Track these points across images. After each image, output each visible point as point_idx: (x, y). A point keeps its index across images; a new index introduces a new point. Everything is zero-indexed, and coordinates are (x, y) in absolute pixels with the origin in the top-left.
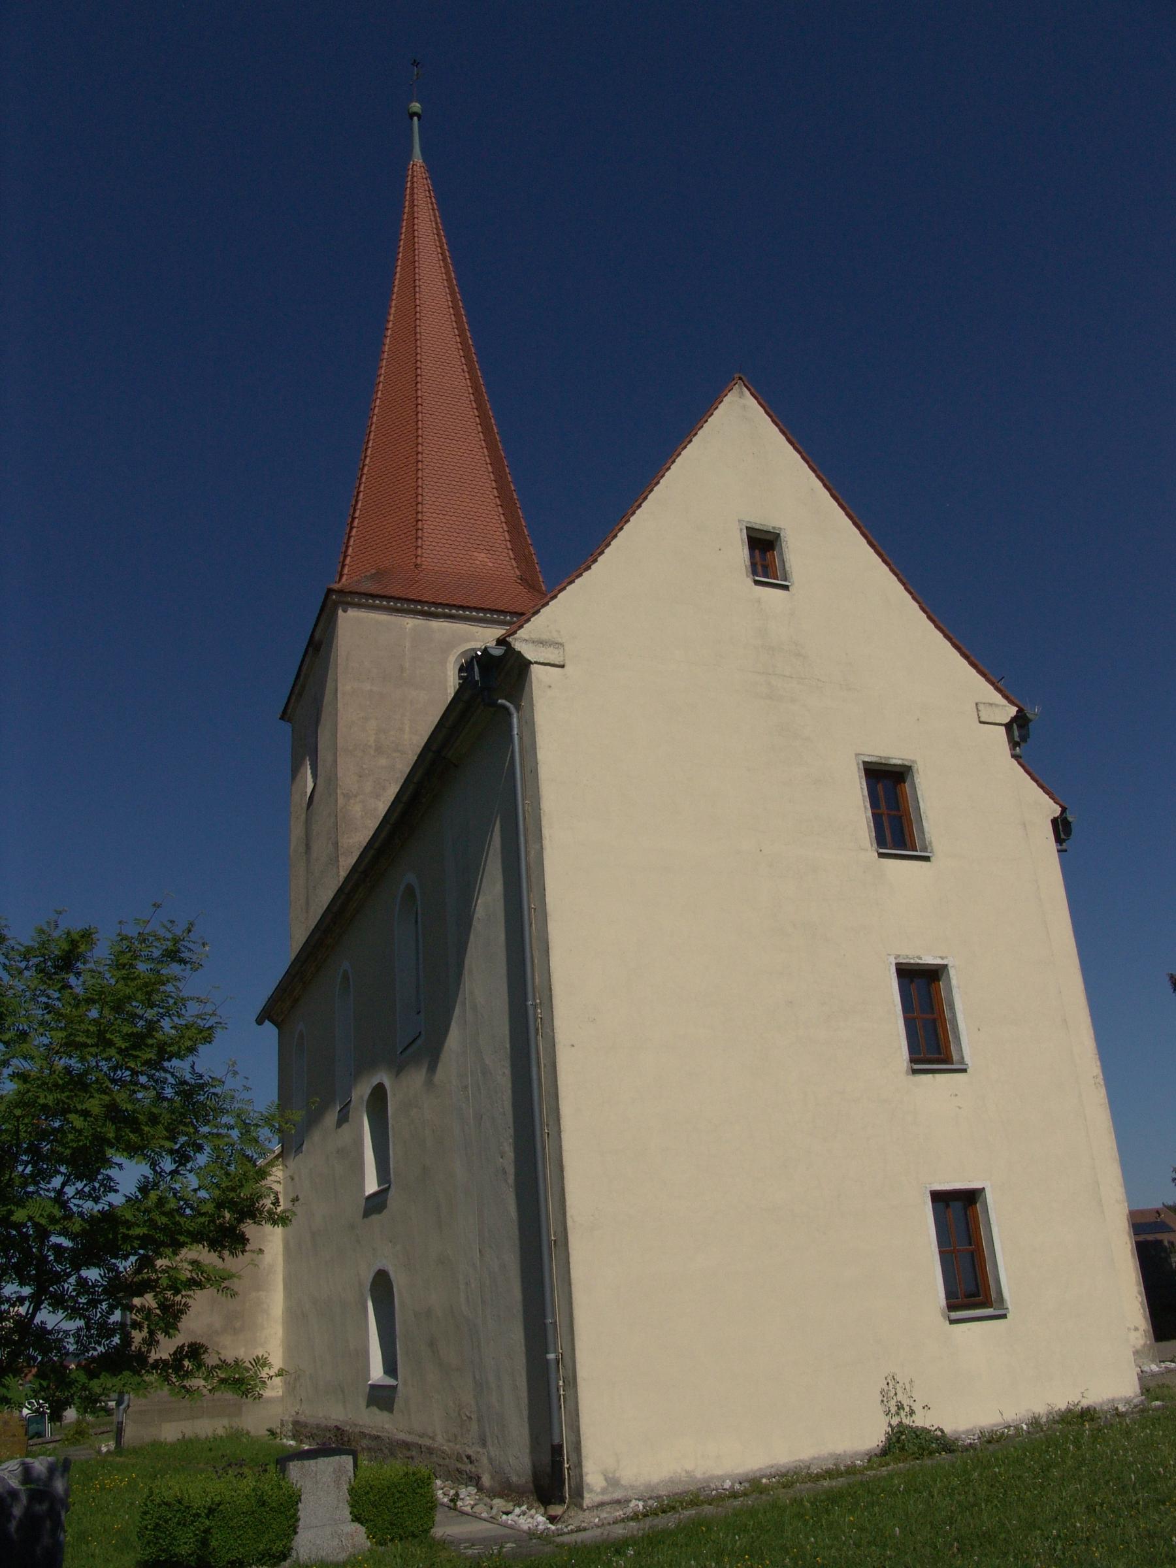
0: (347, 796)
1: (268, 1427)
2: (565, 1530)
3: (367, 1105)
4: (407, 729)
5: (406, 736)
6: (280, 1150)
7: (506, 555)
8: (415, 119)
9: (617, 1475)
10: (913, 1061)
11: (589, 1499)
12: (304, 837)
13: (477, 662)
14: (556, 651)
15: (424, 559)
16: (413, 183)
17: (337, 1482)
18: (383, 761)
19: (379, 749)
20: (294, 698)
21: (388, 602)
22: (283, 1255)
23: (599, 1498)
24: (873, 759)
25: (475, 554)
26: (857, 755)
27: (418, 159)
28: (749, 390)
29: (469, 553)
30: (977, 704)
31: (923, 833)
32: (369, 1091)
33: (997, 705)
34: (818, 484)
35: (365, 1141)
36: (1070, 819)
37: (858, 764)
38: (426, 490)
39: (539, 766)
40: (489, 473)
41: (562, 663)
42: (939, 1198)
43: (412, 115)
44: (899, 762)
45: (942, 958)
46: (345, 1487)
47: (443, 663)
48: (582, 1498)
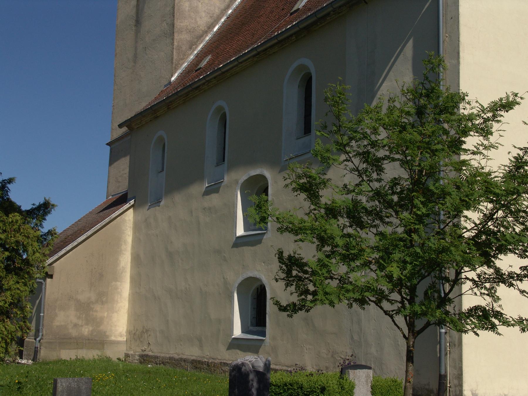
1: (118, 357)
6: (133, 203)
9: (477, 392)
12: (135, 16)
17: (367, 381)
22: (131, 263)
32: (245, 177)
35: (238, 207)
39: (460, 16)
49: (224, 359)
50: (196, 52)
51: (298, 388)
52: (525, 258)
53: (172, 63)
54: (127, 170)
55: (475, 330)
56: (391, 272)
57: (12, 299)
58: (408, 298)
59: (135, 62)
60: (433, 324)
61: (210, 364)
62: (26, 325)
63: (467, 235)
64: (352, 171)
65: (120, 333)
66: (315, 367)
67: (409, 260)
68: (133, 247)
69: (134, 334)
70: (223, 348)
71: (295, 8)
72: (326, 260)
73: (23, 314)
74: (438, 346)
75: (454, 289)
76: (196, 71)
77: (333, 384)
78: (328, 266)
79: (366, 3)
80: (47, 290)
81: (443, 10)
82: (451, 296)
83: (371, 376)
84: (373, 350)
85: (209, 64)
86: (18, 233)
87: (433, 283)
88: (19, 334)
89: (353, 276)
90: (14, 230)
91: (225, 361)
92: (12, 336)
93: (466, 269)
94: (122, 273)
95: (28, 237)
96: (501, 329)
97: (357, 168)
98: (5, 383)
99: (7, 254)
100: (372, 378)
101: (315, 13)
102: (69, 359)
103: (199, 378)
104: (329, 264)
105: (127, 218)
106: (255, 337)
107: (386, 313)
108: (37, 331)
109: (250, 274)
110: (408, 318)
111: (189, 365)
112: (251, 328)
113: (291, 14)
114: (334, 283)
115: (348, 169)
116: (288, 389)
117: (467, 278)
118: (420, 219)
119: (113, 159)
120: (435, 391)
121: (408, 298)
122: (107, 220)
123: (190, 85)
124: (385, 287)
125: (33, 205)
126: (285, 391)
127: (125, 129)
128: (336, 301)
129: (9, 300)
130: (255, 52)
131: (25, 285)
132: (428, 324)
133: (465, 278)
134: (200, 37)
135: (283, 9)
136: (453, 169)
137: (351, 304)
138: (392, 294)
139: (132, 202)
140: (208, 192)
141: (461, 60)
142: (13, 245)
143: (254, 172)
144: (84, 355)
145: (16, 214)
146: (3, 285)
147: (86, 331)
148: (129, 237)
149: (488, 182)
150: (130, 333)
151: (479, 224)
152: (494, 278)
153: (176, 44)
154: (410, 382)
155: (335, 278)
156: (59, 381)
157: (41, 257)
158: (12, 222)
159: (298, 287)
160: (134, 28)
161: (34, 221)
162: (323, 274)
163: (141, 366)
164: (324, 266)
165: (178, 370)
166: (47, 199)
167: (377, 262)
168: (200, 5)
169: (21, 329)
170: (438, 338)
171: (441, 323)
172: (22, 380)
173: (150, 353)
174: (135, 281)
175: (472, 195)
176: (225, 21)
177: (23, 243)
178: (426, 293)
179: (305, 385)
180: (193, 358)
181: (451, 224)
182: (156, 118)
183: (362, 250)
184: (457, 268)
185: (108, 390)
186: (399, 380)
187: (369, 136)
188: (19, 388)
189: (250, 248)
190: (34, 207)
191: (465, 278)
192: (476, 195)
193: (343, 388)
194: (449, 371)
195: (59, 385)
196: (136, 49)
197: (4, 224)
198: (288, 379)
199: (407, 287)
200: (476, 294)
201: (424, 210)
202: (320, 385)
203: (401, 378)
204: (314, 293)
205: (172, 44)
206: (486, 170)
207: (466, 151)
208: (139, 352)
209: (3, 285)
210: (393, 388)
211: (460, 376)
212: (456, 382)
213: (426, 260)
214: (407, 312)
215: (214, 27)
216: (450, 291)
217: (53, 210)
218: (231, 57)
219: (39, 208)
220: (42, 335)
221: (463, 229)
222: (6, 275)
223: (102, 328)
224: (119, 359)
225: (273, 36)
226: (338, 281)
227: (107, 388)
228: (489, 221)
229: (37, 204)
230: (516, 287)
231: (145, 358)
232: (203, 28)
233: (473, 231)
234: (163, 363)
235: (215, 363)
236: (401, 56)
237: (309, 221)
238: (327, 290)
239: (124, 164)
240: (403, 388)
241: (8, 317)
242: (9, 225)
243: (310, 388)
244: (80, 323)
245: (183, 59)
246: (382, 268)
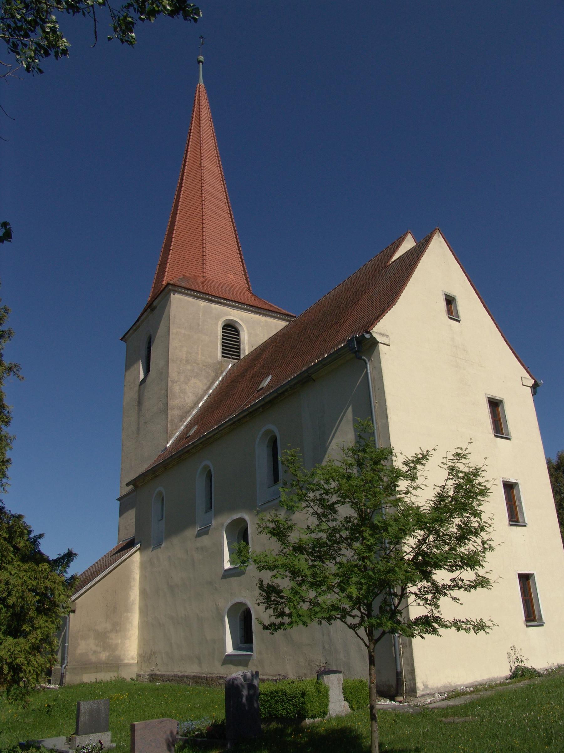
0: (173, 382)
3: (226, 528)
5: (199, 357)
6: (139, 546)
8: (201, 64)
10: (510, 521)
11: (419, 693)
14: (387, 339)
16: (199, 94)
17: (338, 684)
18: (189, 367)
19: (187, 362)
20: (131, 331)
21: (194, 293)
23: (422, 693)
26: (486, 394)
27: (201, 83)
28: (441, 235)
31: (507, 428)
32: (229, 521)
33: (528, 379)
35: (224, 545)
43: (199, 62)
44: (499, 398)
45: (516, 480)
46: (341, 686)
47: (216, 324)
48: (416, 693)
49: (220, 674)
50: (185, 424)
51: (283, 695)
52: (453, 572)
53: (167, 433)
54: (134, 520)
55: (421, 634)
56: (350, 592)
57: (42, 636)
58: (366, 613)
59: (138, 434)
60: (388, 632)
61: (208, 679)
62: (53, 658)
63: (406, 558)
64: (313, 514)
65: (132, 656)
66: (295, 674)
67: (364, 582)
68: (140, 583)
69: (144, 657)
70: (218, 664)
71: (261, 387)
72: (298, 589)
73: (51, 648)
74: (393, 648)
75: (401, 602)
76: (186, 438)
77: (311, 689)
78: (299, 593)
79: (314, 381)
80: (70, 623)
81: (372, 383)
82: (399, 608)
83: (342, 679)
84: (342, 656)
85: (197, 432)
86: (46, 579)
87: (385, 599)
88: (48, 665)
89: (320, 599)
90: (44, 577)
91: (220, 675)
92: (42, 668)
93: (409, 585)
94: (132, 605)
95: (55, 583)
96: (441, 631)
97: (317, 512)
98: (37, 707)
99: (38, 597)
100: (342, 681)
101: (276, 390)
102: (89, 682)
103: (200, 692)
104: (300, 591)
105: (135, 559)
106: (245, 653)
107: (350, 627)
108: (63, 659)
109: (237, 600)
110: (367, 629)
111: (191, 681)
112: (241, 645)
113: (258, 391)
114: (305, 606)
115: (310, 513)
116: (275, 696)
117: (411, 593)
118: (369, 548)
119: (122, 512)
120: (394, 686)
121: (366, 613)
122: (119, 562)
123: (182, 450)
124: (347, 605)
125: (59, 555)
126: (272, 698)
127: (131, 487)
128: (309, 621)
129: (40, 637)
130: (231, 422)
131: (53, 622)
132: (384, 633)
133: (409, 593)
134: (188, 412)
135: (251, 388)
136: (391, 505)
137: (321, 621)
138: (353, 611)
139: (139, 546)
140: (199, 535)
141: (389, 420)
142: (43, 590)
143: (236, 516)
144: (103, 678)
145: (45, 563)
146: (35, 624)
147: (103, 656)
148: (137, 575)
149: (418, 515)
150: (140, 657)
151: (416, 548)
152: (431, 590)
153: (169, 418)
154: (373, 683)
155: (306, 601)
156: (82, 703)
157: (65, 599)
158: (42, 570)
159: (275, 610)
160: (137, 408)
161: (60, 568)
162: (297, 600)
163: (150, 685)
164: (296, 593)
165: (182, 685)
166: (70, 549)
167: (339, 585)
168: (187, 388)
169: (50, 661)
170: (393, 641)
171: (393, 631)
172: (51, 704)
173: (158, 673)
174: (143, 612)
175: (408, 524)
176: (207, 399)
177: (51, 587)
178: (381, 608)
179: (288, 692)
180: (194, 674)
181: (394, 549)
182: (156, 476)
183: (326, 577)
184: (401, 585)
185: (124, 708)
186: (364, 680)
187: (323, 486)
188: (48, 711)
189: (235, 578)
190: (60, 556)
191: (409, 593)
192: (410, 525)
193: (319, 692)
194: (404, 668)
195: (82, 707)
196: (139, 424)
197: (36, 573)
198: (273, 688)
199: (364, 604)
200: (419, 604)
201: (372, 540)
202: (301, 691)
203: (366, 678)
204: (290, 615)
205: (167, 418)
206: (416, 505)
207: (399, 492)
208: (147, 672)
209: (35, 624)
210: (360, 687)
211: (412, 672)
212: (410, 676)
213: (377, 581)
214: (367, 624)
215: (199, 403)
216: (399, 603)
217: (74, 558)
218: (213, 426)
219: (63, 557)
220: (67, 662)
221: (404, 553)
222: (37, 616)
223: (117, 653)
224: (132, 679)
225: (245, 409)
226: (309, 604)
227: (123, 706)
228: (423, 545)
229: (62, 554)
230: (449, 596)
231: (154, 677)
232: (190, 404)
233: (412, 554)
234: (169, 680)
235: (212, 677)
236: (344, 419)
237: (282, 560)
238: (300, 612)
239: (131, 514)
240: (368, 687)
241: (39, 651)
242: (39, 573)
243: (293, 694)
244: (98, 649)
245: (176, 429)
246: (343, 590)
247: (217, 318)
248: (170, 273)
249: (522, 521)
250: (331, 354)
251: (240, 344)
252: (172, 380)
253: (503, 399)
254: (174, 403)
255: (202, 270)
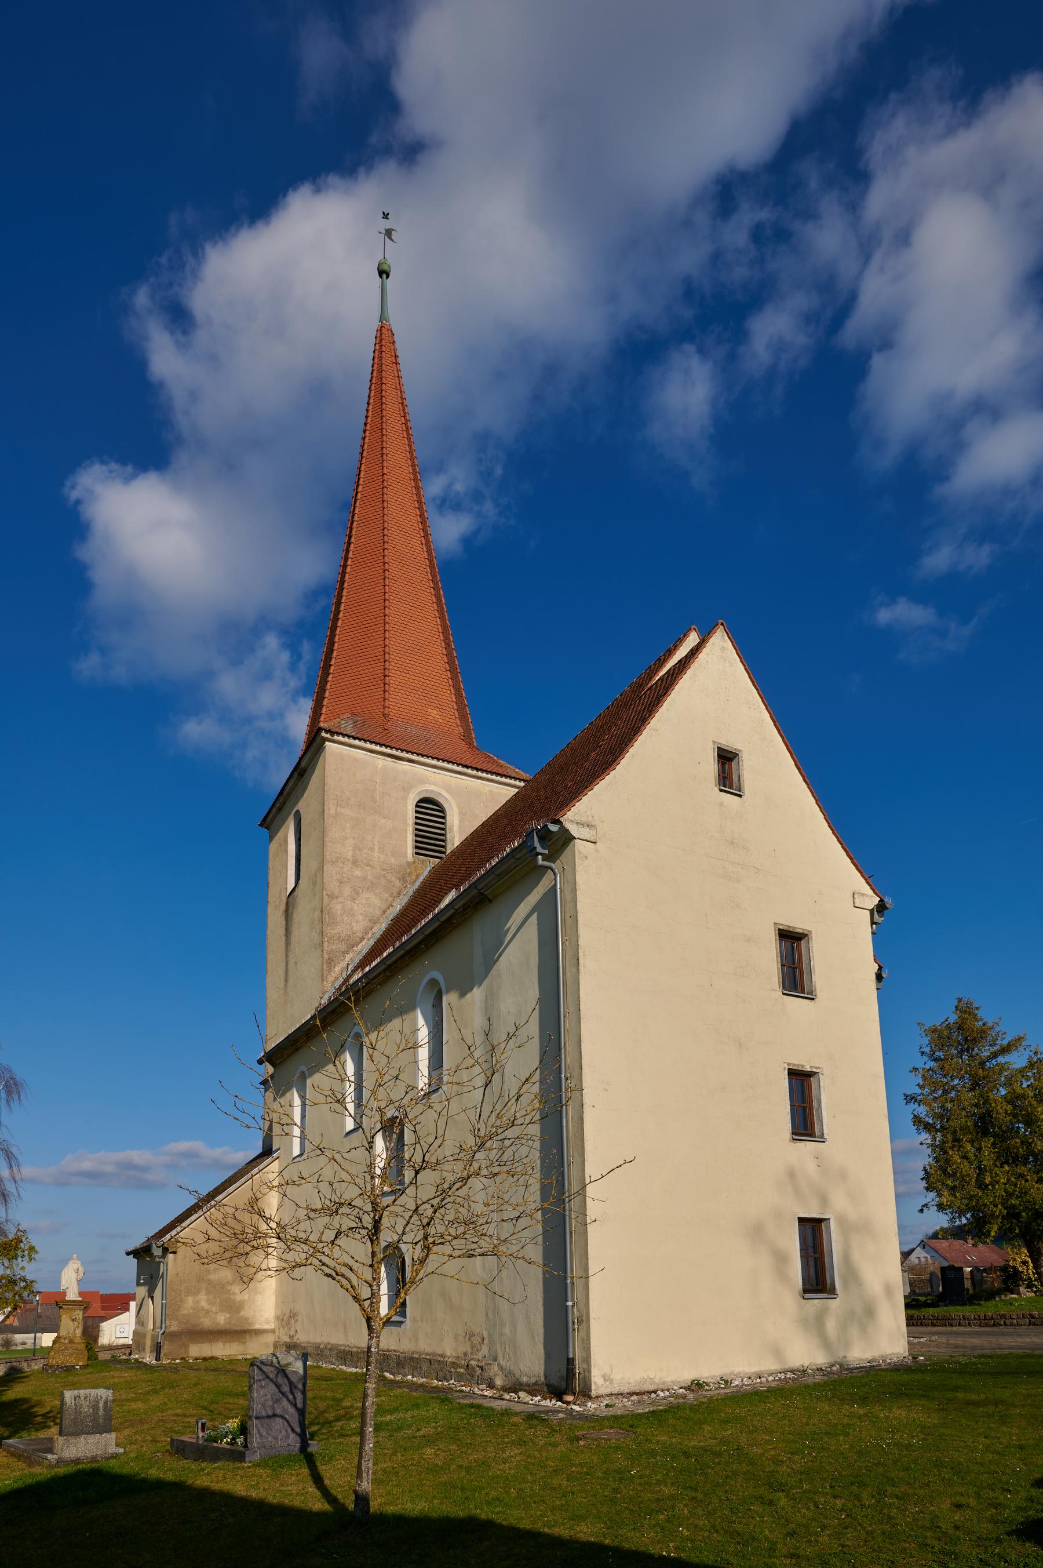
2: (531, 1402)
4: (376, 848)
5: (376, 854)
7: (452, 714)
10: (793, 1133)
13: (536, 833)
15: (390, 710)
18: (358, 873)
19: (355, 863)
20: (274, 811)
24: (785, 928)
25: (429, 710)
28: (728, 634)
29: (425, 709)
30: (854, 894)
33: (868, 896)
34: (766, 716)
36: (883, 975)
37: (775, 931)
38: (392, 650)
40: (441, 640)
41: (595, 841)
42: (801, 1220)
44: (801, 931)
47: (405, 799)
69: (282, 1320)
147: (222, 1319)
211: (587, 1360)
247: (407, 789)
248: (330, 709)
249: (820, 1134)
250: (503, 859)
251: (446, 832)
252: (329, 893)
253: (810, 932)
254: (333, 932)
255: (382, 703)
